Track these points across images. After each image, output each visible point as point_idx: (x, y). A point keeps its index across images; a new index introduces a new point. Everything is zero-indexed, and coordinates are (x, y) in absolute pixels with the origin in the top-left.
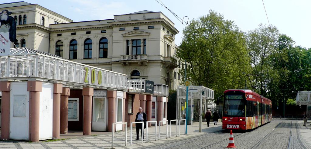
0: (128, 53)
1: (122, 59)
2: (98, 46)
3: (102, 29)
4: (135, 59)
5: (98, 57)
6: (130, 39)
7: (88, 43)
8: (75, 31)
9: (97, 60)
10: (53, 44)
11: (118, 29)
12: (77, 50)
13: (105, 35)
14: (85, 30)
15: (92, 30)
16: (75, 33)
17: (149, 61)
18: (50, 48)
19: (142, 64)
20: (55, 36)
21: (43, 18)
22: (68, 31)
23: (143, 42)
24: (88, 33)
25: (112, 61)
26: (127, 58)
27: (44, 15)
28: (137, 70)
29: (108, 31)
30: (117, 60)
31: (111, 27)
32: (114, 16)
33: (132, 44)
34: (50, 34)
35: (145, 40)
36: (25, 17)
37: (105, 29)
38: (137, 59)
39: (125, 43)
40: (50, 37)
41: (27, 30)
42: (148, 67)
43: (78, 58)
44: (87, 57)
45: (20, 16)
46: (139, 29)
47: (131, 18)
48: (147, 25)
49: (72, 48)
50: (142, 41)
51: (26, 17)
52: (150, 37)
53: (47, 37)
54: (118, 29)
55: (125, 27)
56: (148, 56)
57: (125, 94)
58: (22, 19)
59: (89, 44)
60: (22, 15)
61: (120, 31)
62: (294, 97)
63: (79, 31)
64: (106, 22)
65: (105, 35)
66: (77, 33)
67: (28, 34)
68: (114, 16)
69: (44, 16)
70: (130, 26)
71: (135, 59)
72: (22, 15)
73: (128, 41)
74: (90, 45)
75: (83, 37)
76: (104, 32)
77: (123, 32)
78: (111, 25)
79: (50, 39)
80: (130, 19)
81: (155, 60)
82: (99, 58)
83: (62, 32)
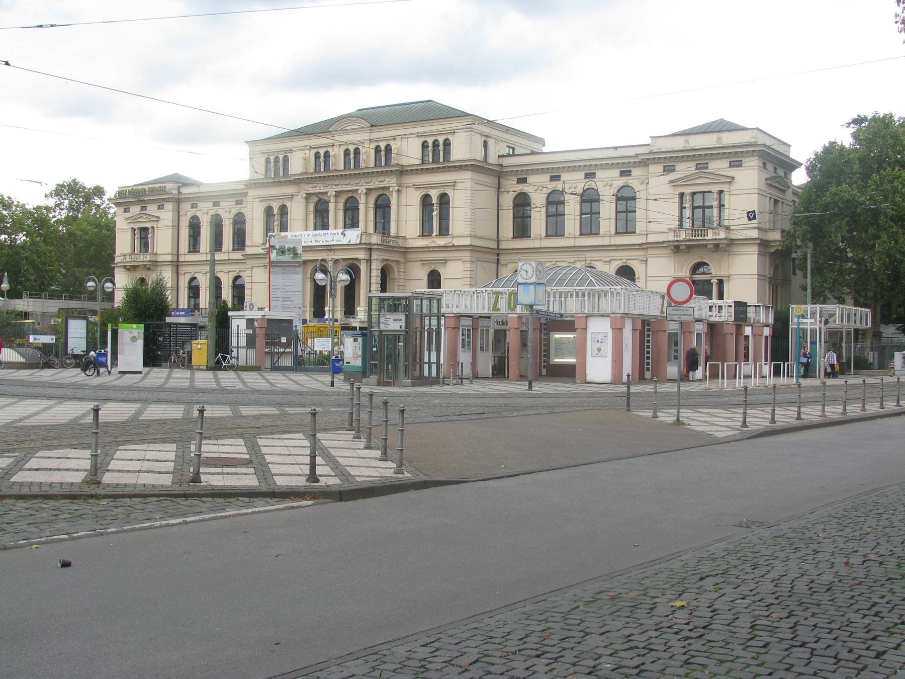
0: (681, 226)
1: (672, 238)
2: (614, 205)
3: (621, 168)
4: (701, 238)
5: (613, 232)
6: (136, 226)
7: (555, 202)
8: (559, 172)
9: (613, 238)
10: (508, 201)
11: (659, 168)
12: (599, 213)
13: (219, 210)
14: (582, 170)
15: (599, 169)
16: (594, 174)
17: (731, 243)
18: (180, 231)
19: (717, 247)
20: (186, 207)
21: (485, 145)
22: (612, 166)
23: (691, 199)
24: (216, 204)
25: (648, 241)
26: (683, 236)
27: (487, 136)
28: (705, 261)
29: (636, 172)
30: (661, 238)
31: (644, 163)
32: (651, 137)
33: (693, 200)
34: (179, 204)
35: (721, 192)
36: (447, 143)
37: (630, 167)
38: (706, 238)
39: (677, 199)
40: (179, 210)
41: (446, 173)
42: (729, 255)
43: (223, 249)
44: (555, 234)
45: (436, 144)
46: (707, 168)
47: (688, 143)
48: (580, 170)
49: (622, 207)
50: (715, 196)
51: (288, 161)
52: (734, 186)
53: (494, 186)
54: (659, 168)
55: (676, 164)
56: (728, 228)
57: (706, 325)
58: (441, 147)
59: (627, 199)
60: (441, 140)
61: (730, 169)
62: (574, 337)
63: (567, 171)
64: (632, 152)
65: (632, 181)
66: (565, 177)
67: (455, 182)
68: (650, 139)
69: (488, 139)
70: (640, 167)
71: (700, 238)
72: (441, 140)
73: (682, 195)
74: (594, 204)
75: (232, 210)
76: (705, 165)
77: (672, 176)
78: (643, 159)
79: (499, 189)
80: (687, 145)
81: (529, 248)
82: (617, 233)
83: (528, 174)
